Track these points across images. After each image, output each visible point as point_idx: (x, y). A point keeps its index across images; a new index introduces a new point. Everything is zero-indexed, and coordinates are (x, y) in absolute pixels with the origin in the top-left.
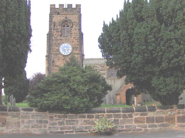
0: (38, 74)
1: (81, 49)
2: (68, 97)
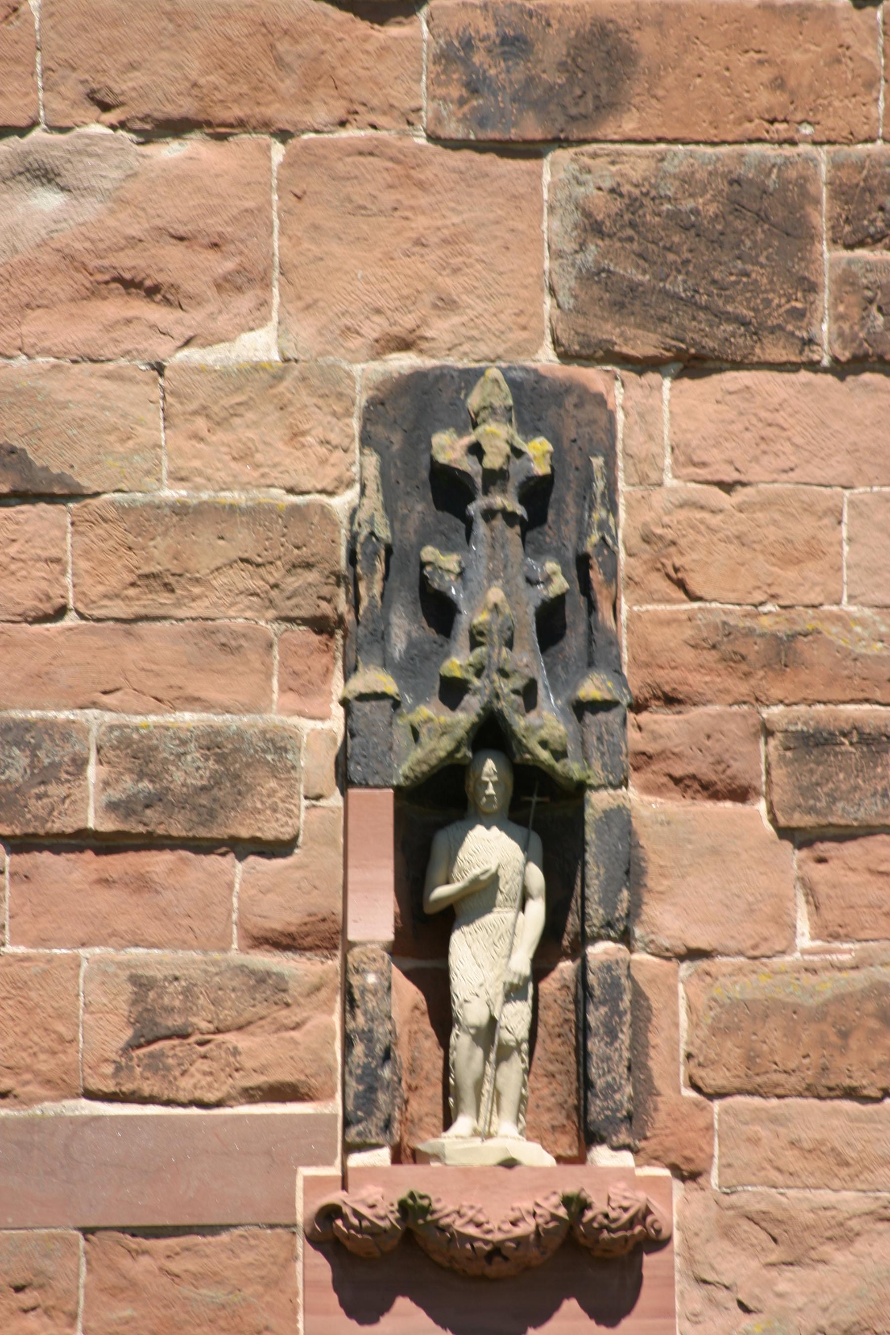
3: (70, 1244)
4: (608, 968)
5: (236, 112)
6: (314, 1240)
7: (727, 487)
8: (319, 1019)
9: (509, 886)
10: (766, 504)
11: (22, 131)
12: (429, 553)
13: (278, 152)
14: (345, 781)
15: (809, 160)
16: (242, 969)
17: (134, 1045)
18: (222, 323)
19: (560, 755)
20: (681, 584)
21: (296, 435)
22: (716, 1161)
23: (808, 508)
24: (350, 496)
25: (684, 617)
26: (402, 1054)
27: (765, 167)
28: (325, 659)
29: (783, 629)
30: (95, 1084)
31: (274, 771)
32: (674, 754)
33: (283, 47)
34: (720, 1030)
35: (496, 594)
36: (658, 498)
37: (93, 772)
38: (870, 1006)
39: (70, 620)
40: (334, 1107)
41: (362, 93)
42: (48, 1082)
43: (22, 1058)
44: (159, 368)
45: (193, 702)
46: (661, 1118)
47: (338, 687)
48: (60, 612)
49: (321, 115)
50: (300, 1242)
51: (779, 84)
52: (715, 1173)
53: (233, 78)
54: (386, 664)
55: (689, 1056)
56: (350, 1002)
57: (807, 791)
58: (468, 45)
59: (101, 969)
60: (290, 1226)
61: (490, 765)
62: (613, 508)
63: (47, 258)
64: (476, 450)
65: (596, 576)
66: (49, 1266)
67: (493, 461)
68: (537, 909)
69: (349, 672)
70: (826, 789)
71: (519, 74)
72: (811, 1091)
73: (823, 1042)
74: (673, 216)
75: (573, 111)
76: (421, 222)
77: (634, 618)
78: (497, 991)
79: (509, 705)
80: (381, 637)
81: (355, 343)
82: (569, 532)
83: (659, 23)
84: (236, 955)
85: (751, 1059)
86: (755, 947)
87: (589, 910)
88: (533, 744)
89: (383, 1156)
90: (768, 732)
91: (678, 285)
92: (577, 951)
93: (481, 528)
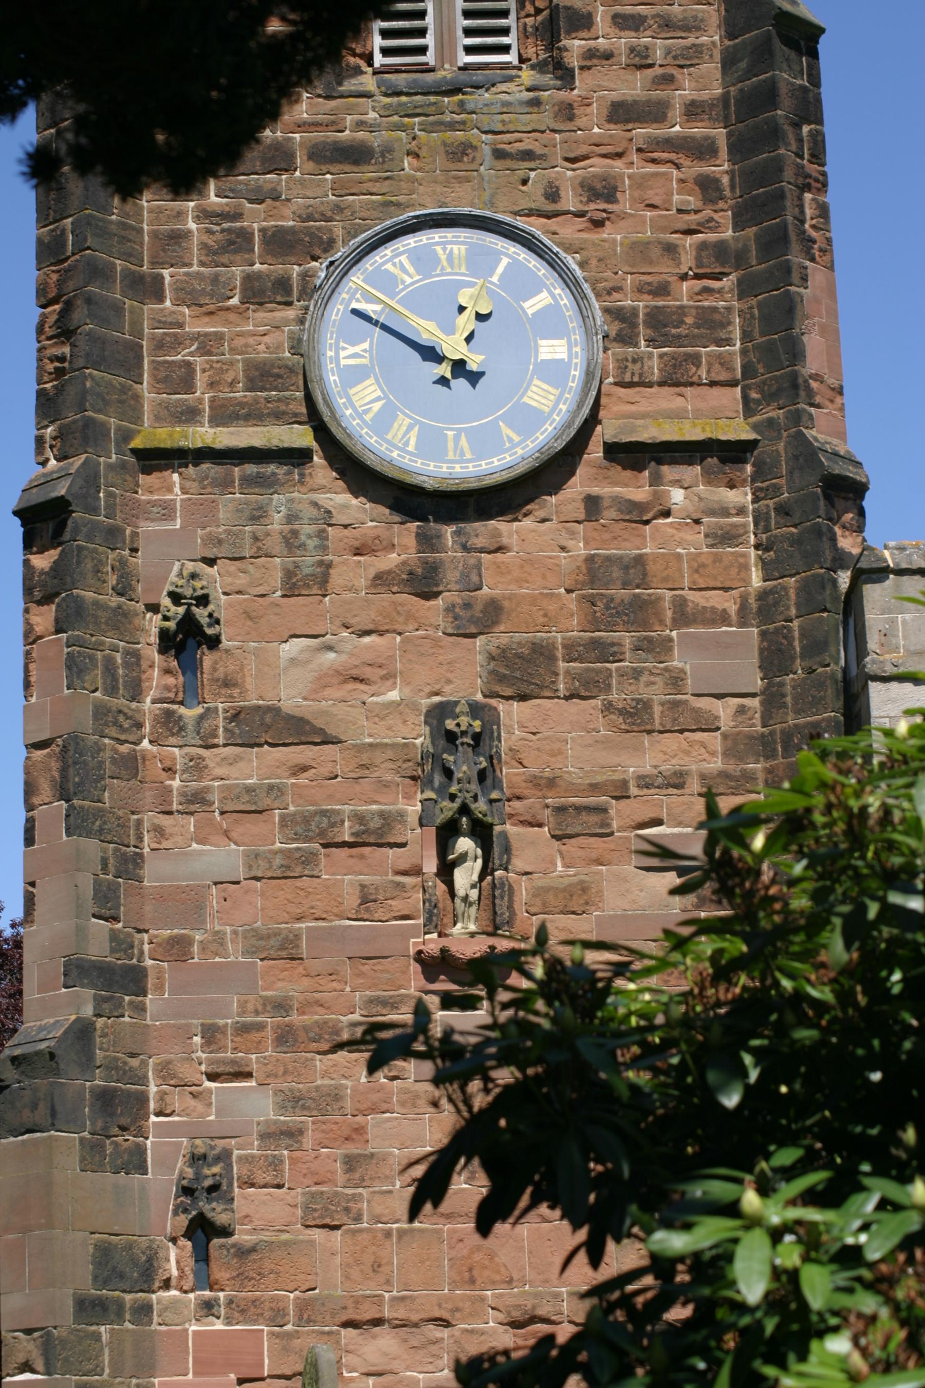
0: (30, 156)
1: (796, 353)
2: (200, 1054)
3: (345, 962)
4: (501, 878)
5: (386, 627)
6: (416, 960)
7: (534, 734)
8: (416, 895)
9: (471, 855)
10: (546, 738)
11: (323, 636)
12: (445, 756)
13: (398, 639)
14: (421, 825)
15: (555, 637)
16: (392, 881)
17: (361, 904)
18: (383, 689)
19: (485, 815)
20: (521, 763)
21: (405, 722)
23: (558, 740)
24: (421, 740)
26: (440, 905)
27: (542, 640)
28: (414, 789)
29: (551, 776)
30: (350, 916)
31: (400, 822)
33: (399, 608)
34: (535, 896)
35: (465, 768)
36: (513, 738)
37: (347, 824)
39: (339, 779)
40: (421, 921)
41: (423, 621)
42: (336, 915)
43: (329, 908)
44: (364, 703)
45: (376, 802)
46: (518, 922)
47: (419, 796)
48: (336, 777)
49: (411, 627)
50: (412, 961)
51: (545, 615)
53: (385, 618)
54: (433, 789)
56: (424, 891)
57: (559, 824)
58: (454, 606)
59: (351, 882)
60: (409, 956)
61: (464, 819)
62: (500, 741)
63: (331, 672)
64: (458, 725)
65: (495, 761)
66: (339, 968)
67: (463, 728)
68: (480, 862)
69: (422, 792)
71: (469, 614)
72: (562, 912)
73: (565, 898)
74: (516, 654)
76: (441, 658)
77: (507, 773)
78: (468, 886)
79: (469, 801)
80: (431, 782)
81: (422, 694)
82: (487, 748)
83: (510, 599)
84: (390, 877)
85: (544, 904)
87: (479, 546)
88: (477, 812)
89: (435, 935)
90: (547, 806)
91: (518, 674)
92: (492, 874)
93: (460, 748)
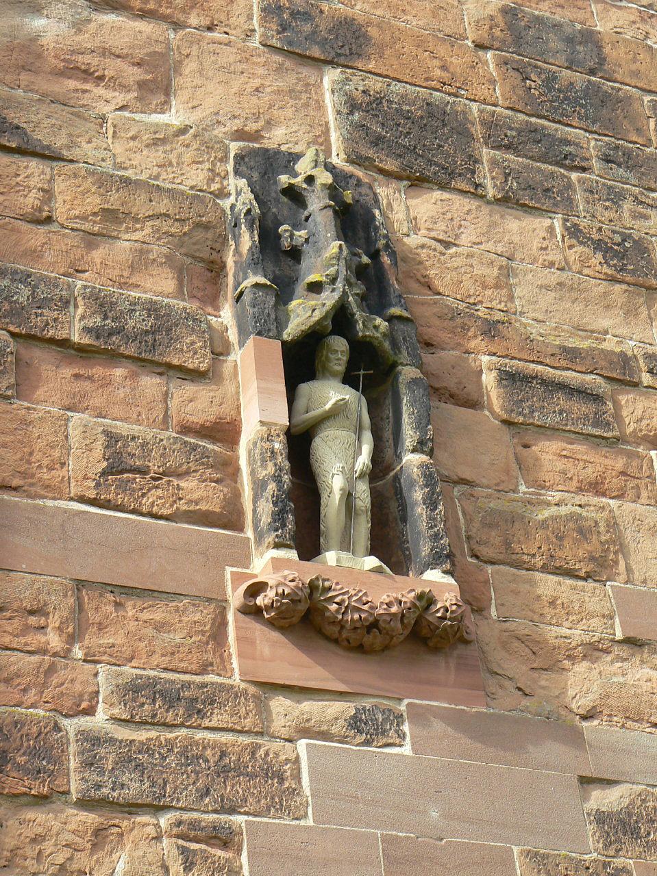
22: (493, 602)
25: (432, 302)
32: (433, 374)
38: (572, 525)
51: (444, 68)
52: (493, 609)
55: (468, 538)
70: (527, 404)
75: (339, 51)
86: (497, 485)
